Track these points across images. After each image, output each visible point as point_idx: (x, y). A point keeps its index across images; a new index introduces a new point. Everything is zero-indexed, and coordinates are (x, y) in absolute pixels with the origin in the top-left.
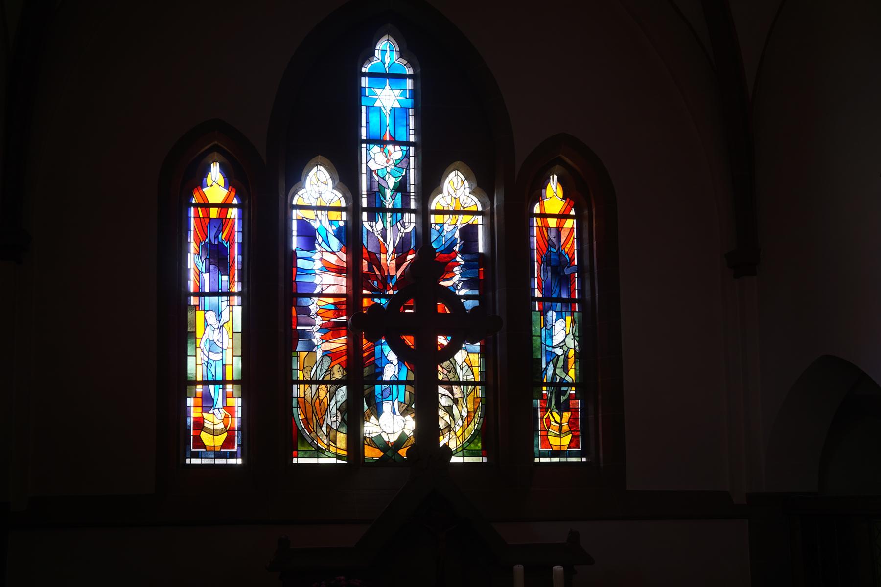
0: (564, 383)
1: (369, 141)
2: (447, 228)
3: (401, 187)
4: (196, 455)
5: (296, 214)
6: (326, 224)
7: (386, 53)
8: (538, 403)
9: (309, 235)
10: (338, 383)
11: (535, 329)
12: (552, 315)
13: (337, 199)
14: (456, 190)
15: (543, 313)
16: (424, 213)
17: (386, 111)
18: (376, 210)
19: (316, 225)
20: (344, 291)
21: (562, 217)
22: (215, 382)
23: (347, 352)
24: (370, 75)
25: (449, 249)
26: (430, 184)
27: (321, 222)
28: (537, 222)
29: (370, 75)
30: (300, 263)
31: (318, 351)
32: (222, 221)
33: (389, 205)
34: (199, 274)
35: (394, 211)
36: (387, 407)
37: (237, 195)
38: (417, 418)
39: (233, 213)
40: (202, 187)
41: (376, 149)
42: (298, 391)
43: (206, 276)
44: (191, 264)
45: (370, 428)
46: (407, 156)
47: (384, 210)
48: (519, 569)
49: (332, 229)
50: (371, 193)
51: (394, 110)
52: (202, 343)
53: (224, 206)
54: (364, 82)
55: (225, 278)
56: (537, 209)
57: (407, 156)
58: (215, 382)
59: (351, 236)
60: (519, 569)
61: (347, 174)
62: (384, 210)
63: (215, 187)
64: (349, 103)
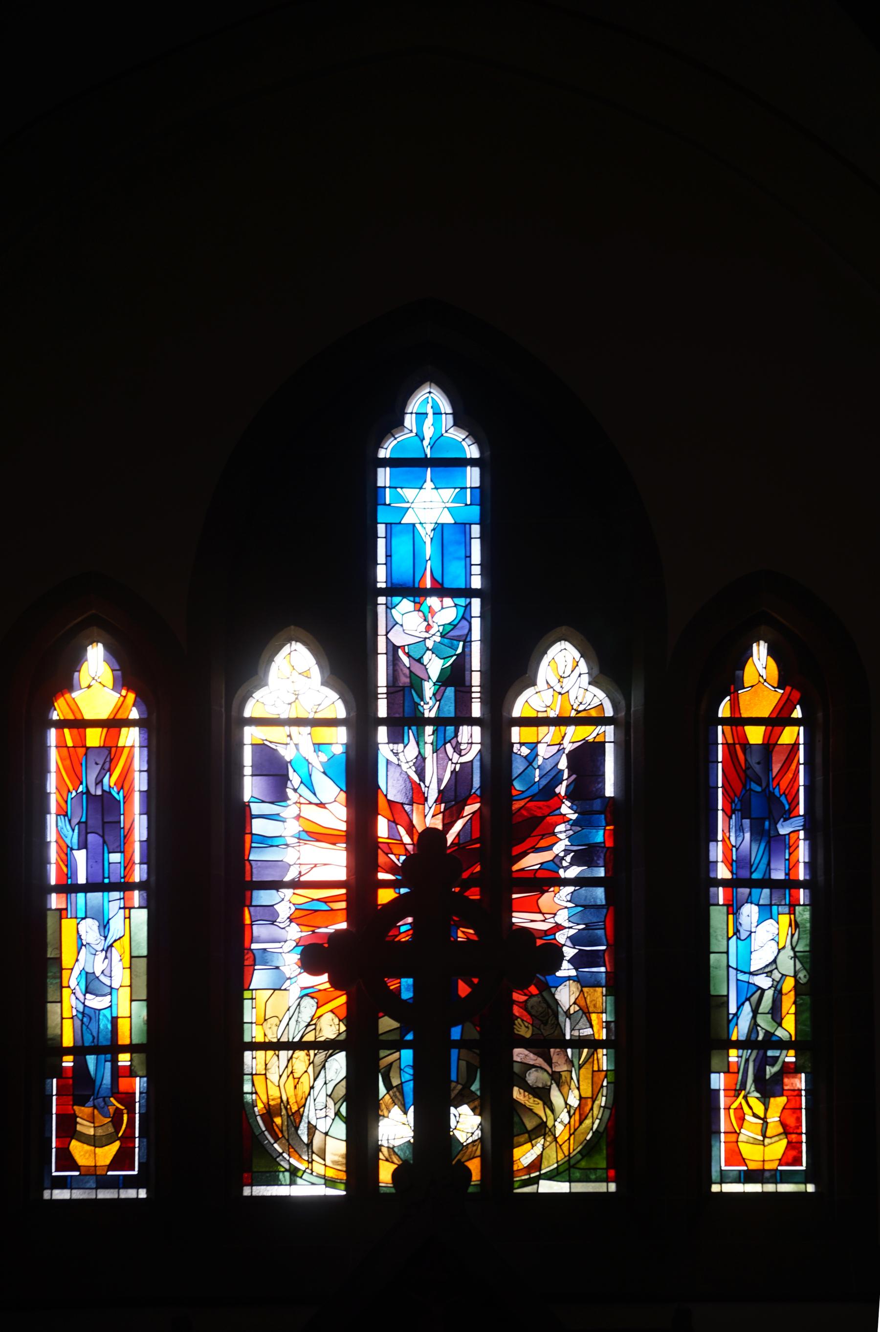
0: (771, 1042)
2: (546, 749)
3: (455, 677)
5: (251, 735)
7: (429, 416)
8: (718, 1081)
9: (276, 772)
10: (331, 1046)
12: (750, 913)
14: (563, 678)
15: (733, 908)
16: (497, 725)
19: (287, 753)
22: (96, 1050)
25: (547, 792)
30: (258, 827)
34: (66, 853)
42: (252, 1061)
43: (80, 856)
46: (466, 617)
49: (317, 761)
51: (440, 528)
52: (73, 980)
53: (114, 724)
54: (384, 477)
56: (724, 710)
61: (348, 659)
63: (96, 686)
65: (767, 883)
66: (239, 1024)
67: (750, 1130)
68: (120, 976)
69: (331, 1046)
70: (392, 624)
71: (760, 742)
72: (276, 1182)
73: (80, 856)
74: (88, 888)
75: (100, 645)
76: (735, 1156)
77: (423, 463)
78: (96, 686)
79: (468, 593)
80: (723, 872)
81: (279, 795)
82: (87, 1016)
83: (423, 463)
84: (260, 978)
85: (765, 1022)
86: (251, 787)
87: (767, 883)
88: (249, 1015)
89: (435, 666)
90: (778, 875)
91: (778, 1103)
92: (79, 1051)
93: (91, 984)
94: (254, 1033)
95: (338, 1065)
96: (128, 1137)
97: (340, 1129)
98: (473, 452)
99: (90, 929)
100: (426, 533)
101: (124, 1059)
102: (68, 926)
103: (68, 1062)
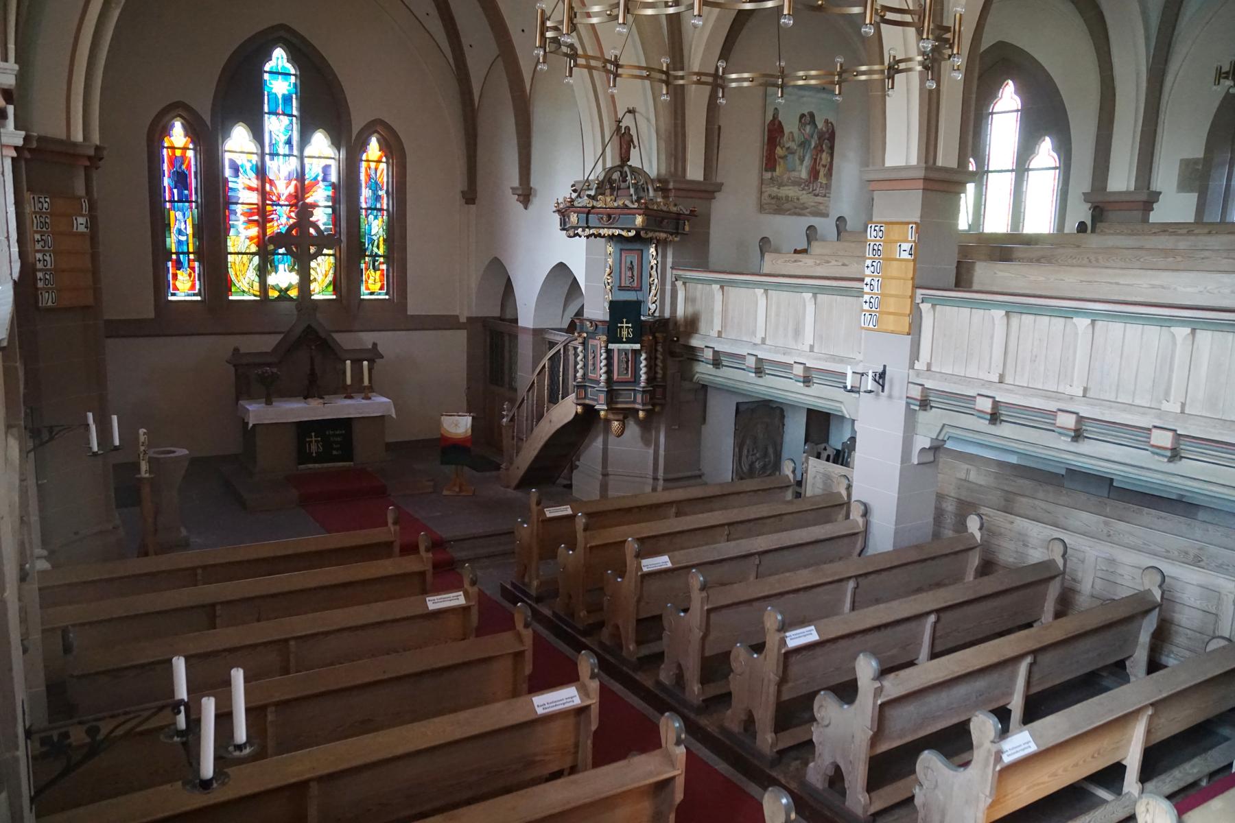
0: (377, 255)
1: (269, 113)
2: (314, 169)
3: (289, 142)
4: (173, 295)
5: (227, 156)
6: (247, 162)
7: (279, 58)
8: (363, 266)
9: (236, 169)
10: (254, 254)
11: (363, 225)
12: (371, 217)
13: (252, 146)
14: (320, 143)
15: (367, 216)
16: (301, 158)
17: (280, 97)
18: (273, 155)
19: (239, 163)
20: (255, 201)
21: (379, 161)
22: (183, 253)
23: (258, 237)
24: (270, 72)
25: (315, 179)
26: (305, 139)
27: (241, 160)
28: (364, 164)
29: (270, 72)
30: (231, 185)
31: (241, 237)
32: (183, 156)
33: (281, 151)
34: (171, 190)
35: (285, 155)
36: (281, 267)
37: (192, 141)
38: (298, 273)
39: (190, 154)
40: (676, 323)
41: (273, 118)
42: (231, 258)
43: (175, 191)
44: (166, 184)
45: (272, 279)
46: (291, 123)
47: (278, 155)
48: (348, 362)
49: (248, 165)
50: (271, 145)
51: (284, 95)
52: (174, 230)
53: (185, 149)
54: (266, 76)
55: (1227, 291)
56: (364, 157)
57: (291, 123)
58: (183, 253)
59: (261, 172)
60: (348, 362)
61: (257, 133)
62: (278, 155)
63: (178, 136)
64: (255, 89)
65: (376, 209)
66: (226, 246)
67: (371, 281)
68: (190, 231)
69: (254, 254)
70: (289, 128)
71: (891, 548)
72: (16, 760)
73: (175, 191)
74: (179, 201)
75: (1047, 139)
76: (367, 288)
77: (278, 73)
78: (178, 136)
79: (292, 116)
80: (364, 205)
81: (237, 176)
82: (180, 243)
83: (278, 73)
84: (232, 232)
85: (375, 250)
86: (228, 173)
87: (376, 209)
88: (229, 243)
89: (284, 138)
90: (378, 206)
91: (378, 273)
92: (178, 253)
93: (180, 232)
94: (231, 249)
95: (256, 259)
96: (194, 281)
97: (257, 279)
98: (293, 71)
99: (179, 215)
100: (280, 97)
101: (192, 256)
102: (172, 213)
103: (174, 257)
